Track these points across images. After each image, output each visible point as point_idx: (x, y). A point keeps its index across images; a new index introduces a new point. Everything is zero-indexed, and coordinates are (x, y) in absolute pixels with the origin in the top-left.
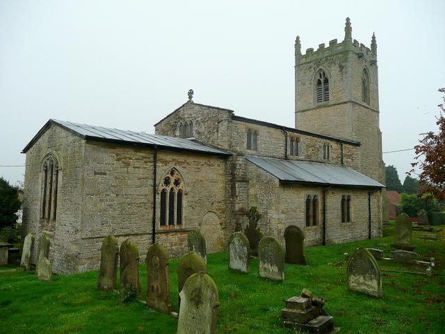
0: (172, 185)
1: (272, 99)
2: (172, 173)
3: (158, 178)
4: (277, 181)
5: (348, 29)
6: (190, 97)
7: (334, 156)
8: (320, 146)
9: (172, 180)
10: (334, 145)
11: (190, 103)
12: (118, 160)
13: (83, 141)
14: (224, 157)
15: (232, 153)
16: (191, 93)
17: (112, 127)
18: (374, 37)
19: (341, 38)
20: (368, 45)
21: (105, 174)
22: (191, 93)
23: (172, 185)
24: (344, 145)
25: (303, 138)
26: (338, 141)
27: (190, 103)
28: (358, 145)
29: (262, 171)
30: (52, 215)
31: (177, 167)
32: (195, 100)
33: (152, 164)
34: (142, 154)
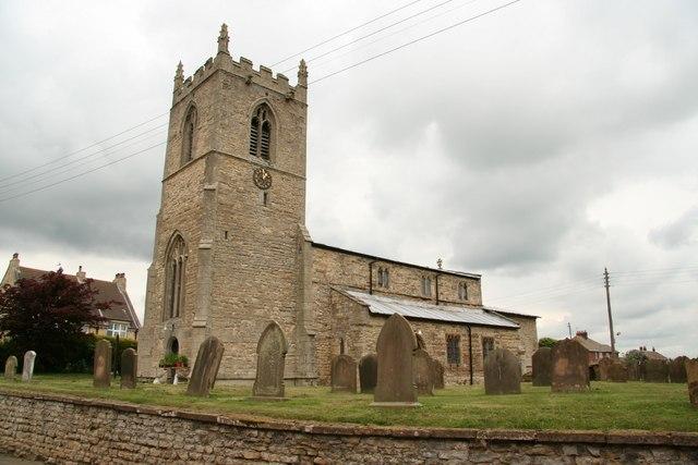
5: (224, 39)
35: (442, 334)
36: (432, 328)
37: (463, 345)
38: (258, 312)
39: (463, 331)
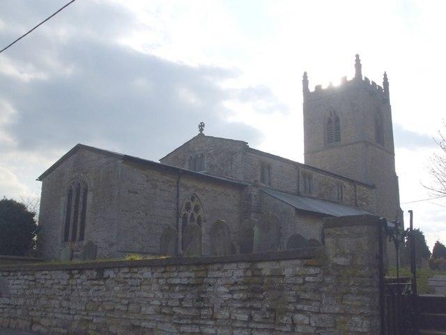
0: (192, 211)
1: (284, 139)
2: (193, 199)
3: (181, 202)
4: (293, 209)
5: (358, 66)
6: (201, 130)
7: (348, 197)
8: (332, 185)
9: (193, 205)
10: (346, 184)
11: (201, 135)
12: (148, 181)
13: (120, 162)
14: (240, 187)
15: (247, 184)
16: (202, 126)
17: (136, 156)
18: (385, 75)
19: (351, 76)
20: (380, 83)
21: (137, 193)
22: (202, 126)
23: (192, 211)
24: (358, 186)
25: (315, 175)
26: (352, 181)
27: (201, 135)
28: (373, 187)
29: (277, 201)
30: (78, 235)
31: (197, 194)
32: (206, 133)
33: (176, 188)
34: (167, 178)
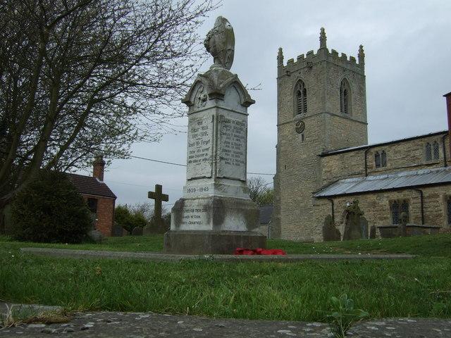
5: (323, 38)
35: (384, 201)
36: (373, 198)
37: (414, 209)
38: (301, 205)
39: (414, 194)
